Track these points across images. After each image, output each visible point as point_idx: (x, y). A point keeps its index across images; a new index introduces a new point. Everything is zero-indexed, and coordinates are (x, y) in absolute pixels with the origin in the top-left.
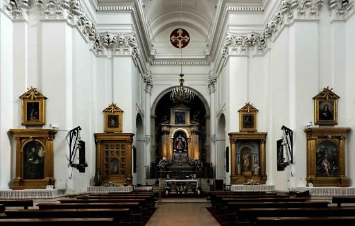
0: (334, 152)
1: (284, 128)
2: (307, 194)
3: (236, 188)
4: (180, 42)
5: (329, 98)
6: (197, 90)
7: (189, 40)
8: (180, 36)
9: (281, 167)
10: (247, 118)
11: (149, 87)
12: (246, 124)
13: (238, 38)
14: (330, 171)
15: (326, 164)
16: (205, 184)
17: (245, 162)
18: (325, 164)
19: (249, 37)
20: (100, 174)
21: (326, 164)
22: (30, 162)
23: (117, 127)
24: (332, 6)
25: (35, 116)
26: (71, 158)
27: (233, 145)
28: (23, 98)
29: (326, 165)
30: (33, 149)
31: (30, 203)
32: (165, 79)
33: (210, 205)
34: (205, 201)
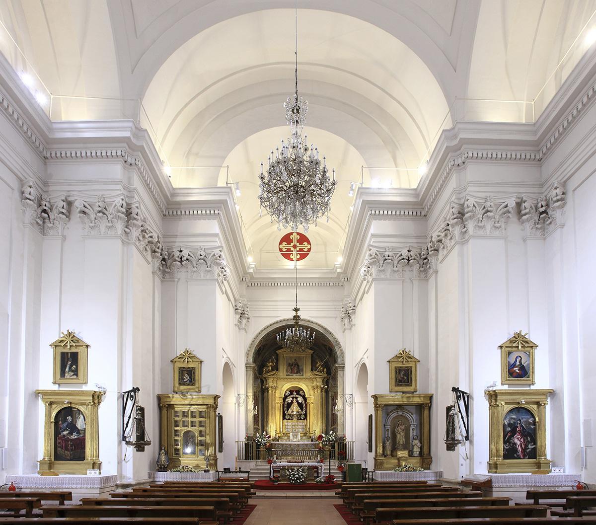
0: (530, 423)
1: (455, 390)
2: (487, 485)
3: (380, 476)
4: (301, 247)
5: (523, 347)
6: (323, 325)
7: (309, 250)
8: (295, 242)
9: (451, 445)
10: (402, 373)
11: (244, 321)
12: (400, 381)
13: (387, 254)
14: (524, 450)
15: (517, 441)
16: (329, 468)
17: (398, 436)
18: (516, 441)
19: (405, 253)
20: (166, 454)
21: (517, 441)
22: (64, 436)
23: (194, 384)
24: (524, 217)
25: (73, 371)
26: (124, 432)
27: (380, 412)
28: (55, 346)
29: (518, 443)
30: (69, 418)
31: (68, 496)
32: (276, 310)
33: (340, 502)
34: (333, 494)
